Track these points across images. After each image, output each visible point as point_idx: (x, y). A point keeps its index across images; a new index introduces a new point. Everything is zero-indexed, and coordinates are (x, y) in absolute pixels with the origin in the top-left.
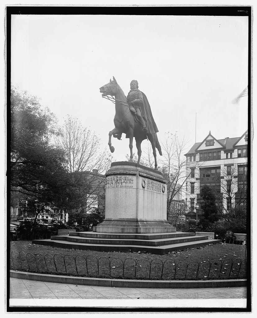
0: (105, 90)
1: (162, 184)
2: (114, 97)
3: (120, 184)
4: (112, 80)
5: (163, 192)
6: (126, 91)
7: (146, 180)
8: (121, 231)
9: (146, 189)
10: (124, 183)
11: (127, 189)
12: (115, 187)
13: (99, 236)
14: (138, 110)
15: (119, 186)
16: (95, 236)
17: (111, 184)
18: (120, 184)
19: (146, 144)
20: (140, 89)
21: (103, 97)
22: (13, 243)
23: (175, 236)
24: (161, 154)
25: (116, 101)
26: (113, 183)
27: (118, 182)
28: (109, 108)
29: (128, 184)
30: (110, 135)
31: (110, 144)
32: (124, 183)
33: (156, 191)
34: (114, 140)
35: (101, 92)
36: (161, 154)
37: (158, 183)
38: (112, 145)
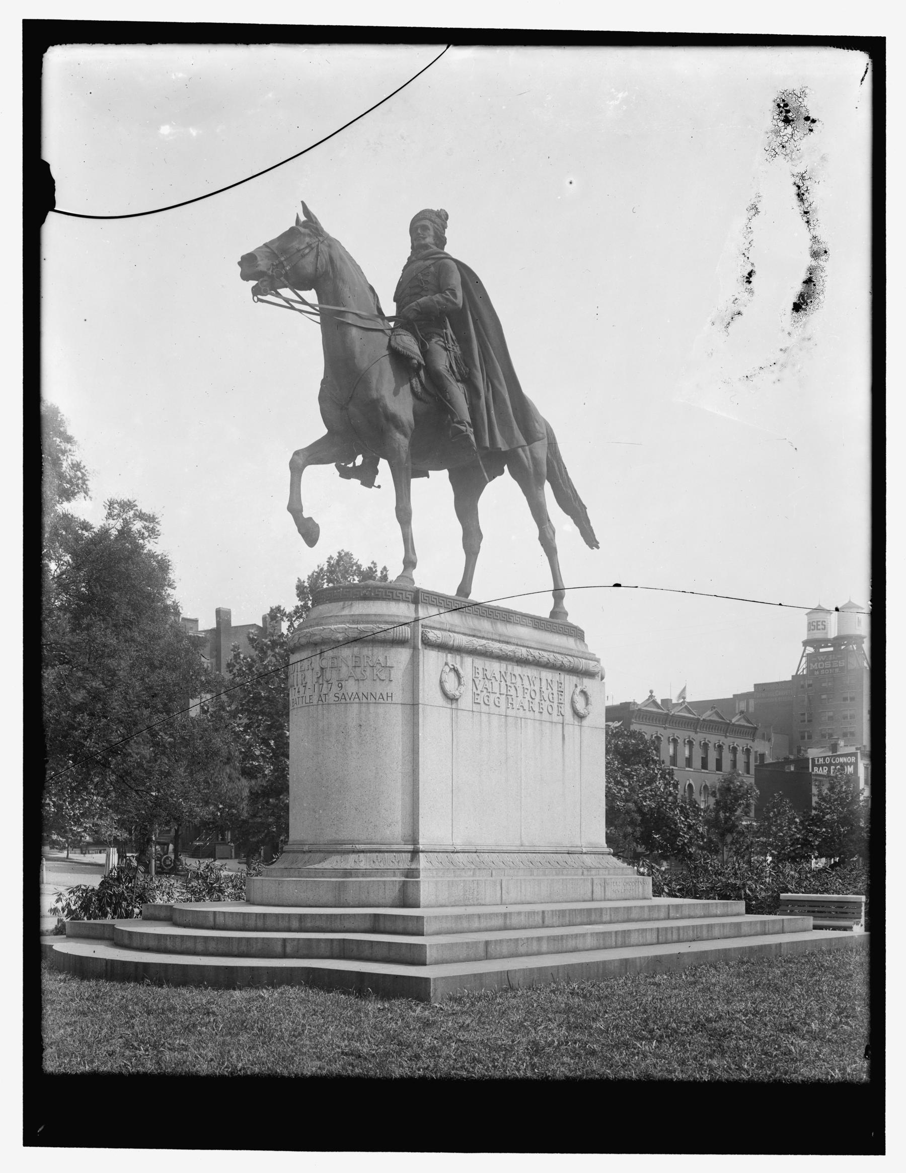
0: (263, 264)
1: (569, 681)
2: (311, 296)
3: (335, 689)
4: (303, 218)
5: (580, 717)
6: (381, 265)
7: (467, 665)
8: (329, 897)
9: (466, 702)
10: (351, 682)
11: (364, 709)
12: (315, 702)
13: (745, 929)
14: (435, 345)
15: (331, 695)
16: (295, 924)
17: (302, 689)
18: (335, 689)
19: (502, 495)
20: (452, 249)
21: (259, 300)
22: (857, 1068)
23: (606, 918)
24: (591, 540)
25: (322, 313)
26: (309, 686)
27: (328, 675)
28: (292, 341)
29: (366, 687)
30: (296, 469)
31: (295, 508)
32: (351, 682)
33: (529, 714)
34: (322, 478)
35: (245, 277)
36: (591, 540)
37: (546, 674)
38: (306, 515)
